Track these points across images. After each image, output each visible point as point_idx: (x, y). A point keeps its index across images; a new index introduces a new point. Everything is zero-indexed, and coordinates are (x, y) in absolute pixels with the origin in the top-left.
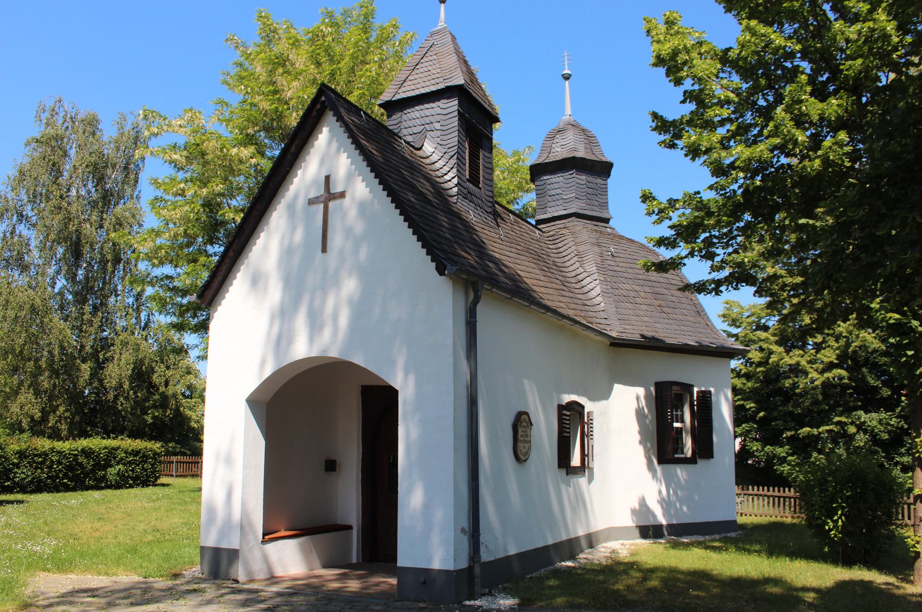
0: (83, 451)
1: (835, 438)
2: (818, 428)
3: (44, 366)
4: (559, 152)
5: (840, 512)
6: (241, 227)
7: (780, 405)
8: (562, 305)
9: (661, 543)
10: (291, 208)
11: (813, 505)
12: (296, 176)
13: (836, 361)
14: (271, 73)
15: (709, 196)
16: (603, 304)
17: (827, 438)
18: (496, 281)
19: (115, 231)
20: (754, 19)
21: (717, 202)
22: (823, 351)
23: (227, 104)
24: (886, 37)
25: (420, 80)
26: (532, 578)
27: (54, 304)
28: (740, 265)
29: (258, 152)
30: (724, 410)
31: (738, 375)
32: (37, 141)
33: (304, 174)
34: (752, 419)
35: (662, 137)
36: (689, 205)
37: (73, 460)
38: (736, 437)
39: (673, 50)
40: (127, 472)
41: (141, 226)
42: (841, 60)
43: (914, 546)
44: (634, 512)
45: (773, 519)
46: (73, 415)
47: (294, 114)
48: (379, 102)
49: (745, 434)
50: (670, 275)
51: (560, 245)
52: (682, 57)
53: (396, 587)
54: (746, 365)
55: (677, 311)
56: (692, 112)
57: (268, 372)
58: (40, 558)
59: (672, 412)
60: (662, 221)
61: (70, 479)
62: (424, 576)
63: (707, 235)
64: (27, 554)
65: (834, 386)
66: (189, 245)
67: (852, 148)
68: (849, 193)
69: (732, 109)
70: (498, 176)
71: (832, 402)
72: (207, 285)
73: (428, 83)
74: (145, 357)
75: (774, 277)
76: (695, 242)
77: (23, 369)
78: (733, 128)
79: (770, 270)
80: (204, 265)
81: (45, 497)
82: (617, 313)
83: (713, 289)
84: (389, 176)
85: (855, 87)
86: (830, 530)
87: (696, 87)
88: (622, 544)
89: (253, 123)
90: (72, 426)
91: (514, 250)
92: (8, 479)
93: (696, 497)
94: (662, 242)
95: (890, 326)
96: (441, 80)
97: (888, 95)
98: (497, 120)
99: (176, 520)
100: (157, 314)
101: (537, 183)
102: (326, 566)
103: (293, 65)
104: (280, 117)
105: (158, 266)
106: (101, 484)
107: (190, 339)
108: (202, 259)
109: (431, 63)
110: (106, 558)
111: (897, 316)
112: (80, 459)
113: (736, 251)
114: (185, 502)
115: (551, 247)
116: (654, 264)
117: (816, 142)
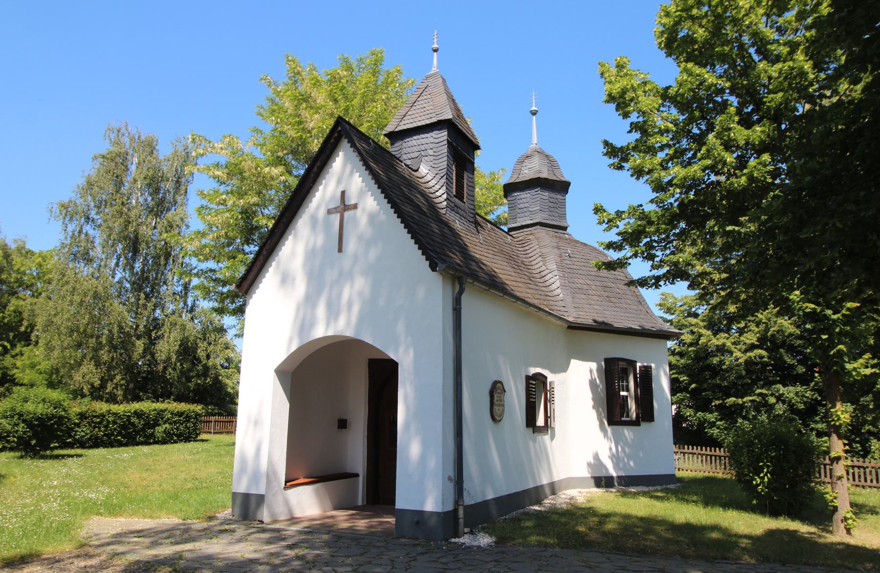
0: (135, 412)
1: (757, 407)
2: (742, 398)
3: (104, 342)
4: (527, 174)
5: (765, 470)
6: (272, 232)
7: (709, 379)
8: (529, 295)
9: (612, 492)
10: (314, 220)
11: (742, 464)
12: (318, 190)
13: (756, 343)
14: (297, 107)
15: (649, 208)
16: (561, 295)
17: (750, 406)
18: (477, 276)
19: (167, 232)
20: (691, 61)
21: (656, 213)
22: (745, 335)
23: (261, 131)
24: (803, 74)
25: (417, 115)
26: (505, 519)
27: (113, 291)
28: (676, 264)
29: (287, 172)
30: (663, 382)
31: (673, 353)
32: (103, 157)
33: (325, 189)
34: (685, 389)
35: (612, 161)
36: (633, 215)
37: (127, 420)
38: (672, 404)
39: (622, 89)
40: (172, 430)
41: (188, 226)
42: (764, 93)
43: (832, 501)
44: (589, 464)
45: (706, 474)
46: (128, 382)
47: (316, 141)
48: (384, 132)
49: (679, 402)
50: (618, 273)
51: (527, 248)
52: (630, 95)
53: (394, 527)
54: (679, 345)
55: (622, 301)
56: (637, 140)
57: (294, 348)
58: (95, 503)
59: (619, 383)
60: (611, 228)
61: (123, 437)
62: (419, 517)
63: (648, 239)
64: (83, 500)
65: (756, 364)
66: (229, 245)
67: (773, 167)
68: (774, 203)
69: (671, 136)
70: (478, 192)
71: (754, 377)
72: (244, 278)
73: (423, 118)
74: (191, 335)
75: (704, 274)
76: (638, 246)
77: (86, 344)
78: (671, 152)
79: (699, 268)
80: (242, 261)
81: (101, 452)
82: (573, 302)
83: (653, 284)
84: (393, 192)
85: (776, 116)
86: (758, 485)
87: (641, 119)
88: (580, 492)
89: (282, 148)
90: (126, 391)
91: (491, 252)
92: (70, 437)
93: (641, 454)
94: (610, 246)
95: (806, 314)
96: (434, 114)
97: (805, 123)
98: (478, 148)
99: (213, 470)
100: (202, 300)
101: (509, 199)
102: (336, 508)
103: (315, 101)
104: (304, 143)
105: (203, 261)
106: (150, 440)
107: (228, 321)
108: (240, 256)
109: (426, 101)
110: (151, 503)
111: (813, 306)
112: (133, 420)
113: (673, 253)
114: (221, 455)
115: (520, 249)
116: (604, 263)
117: (742, 163)
